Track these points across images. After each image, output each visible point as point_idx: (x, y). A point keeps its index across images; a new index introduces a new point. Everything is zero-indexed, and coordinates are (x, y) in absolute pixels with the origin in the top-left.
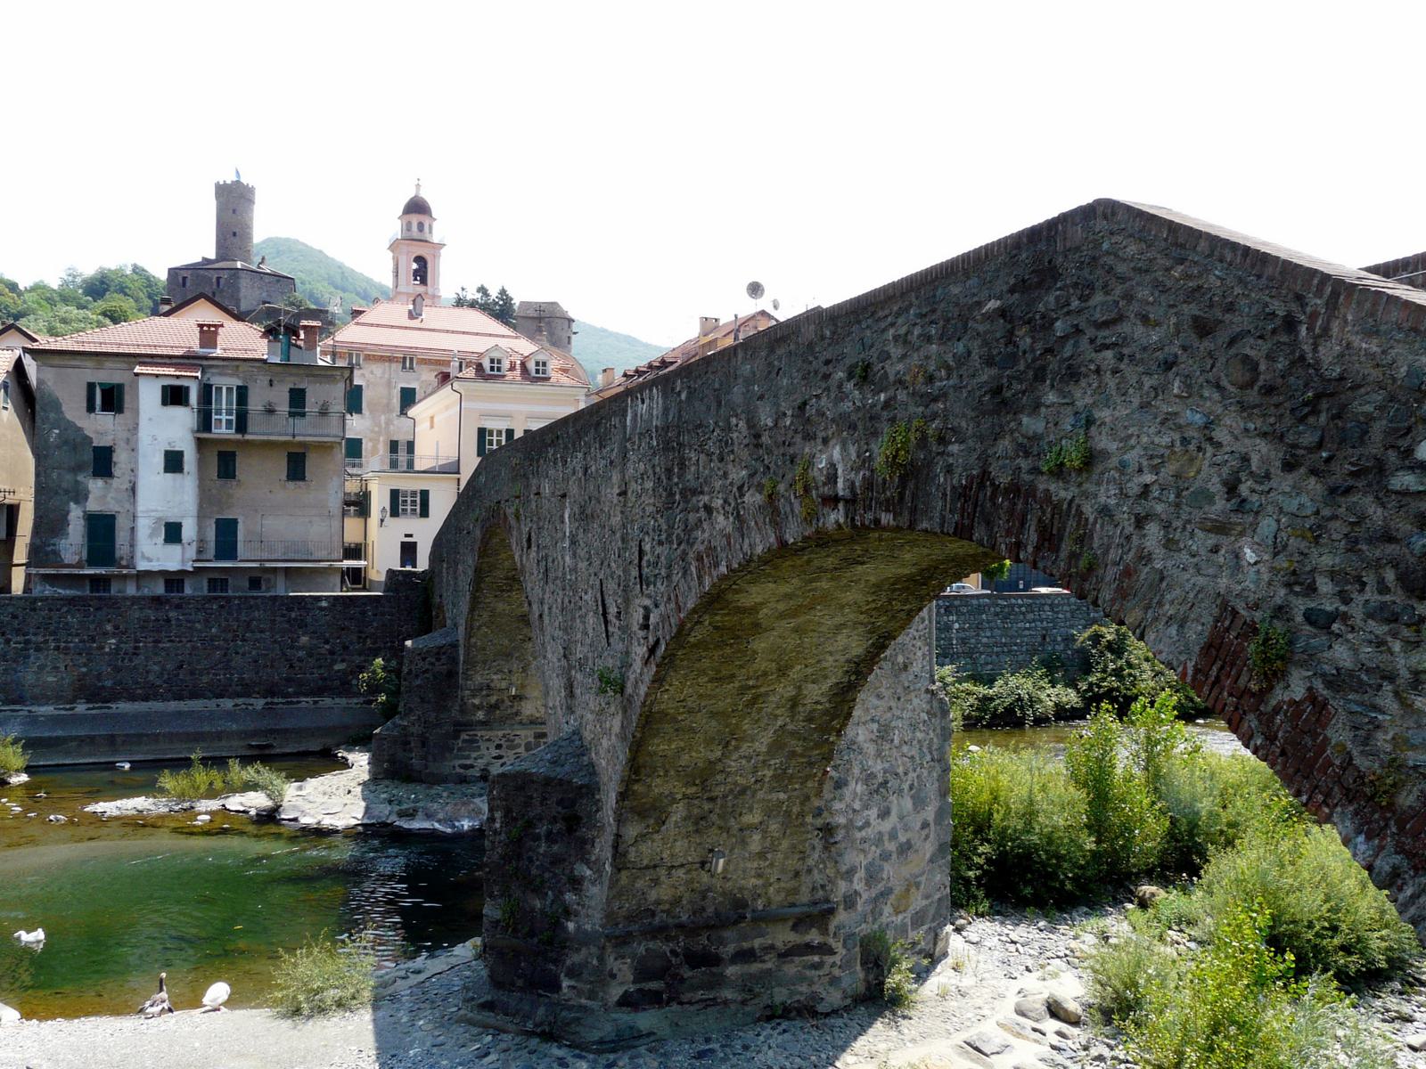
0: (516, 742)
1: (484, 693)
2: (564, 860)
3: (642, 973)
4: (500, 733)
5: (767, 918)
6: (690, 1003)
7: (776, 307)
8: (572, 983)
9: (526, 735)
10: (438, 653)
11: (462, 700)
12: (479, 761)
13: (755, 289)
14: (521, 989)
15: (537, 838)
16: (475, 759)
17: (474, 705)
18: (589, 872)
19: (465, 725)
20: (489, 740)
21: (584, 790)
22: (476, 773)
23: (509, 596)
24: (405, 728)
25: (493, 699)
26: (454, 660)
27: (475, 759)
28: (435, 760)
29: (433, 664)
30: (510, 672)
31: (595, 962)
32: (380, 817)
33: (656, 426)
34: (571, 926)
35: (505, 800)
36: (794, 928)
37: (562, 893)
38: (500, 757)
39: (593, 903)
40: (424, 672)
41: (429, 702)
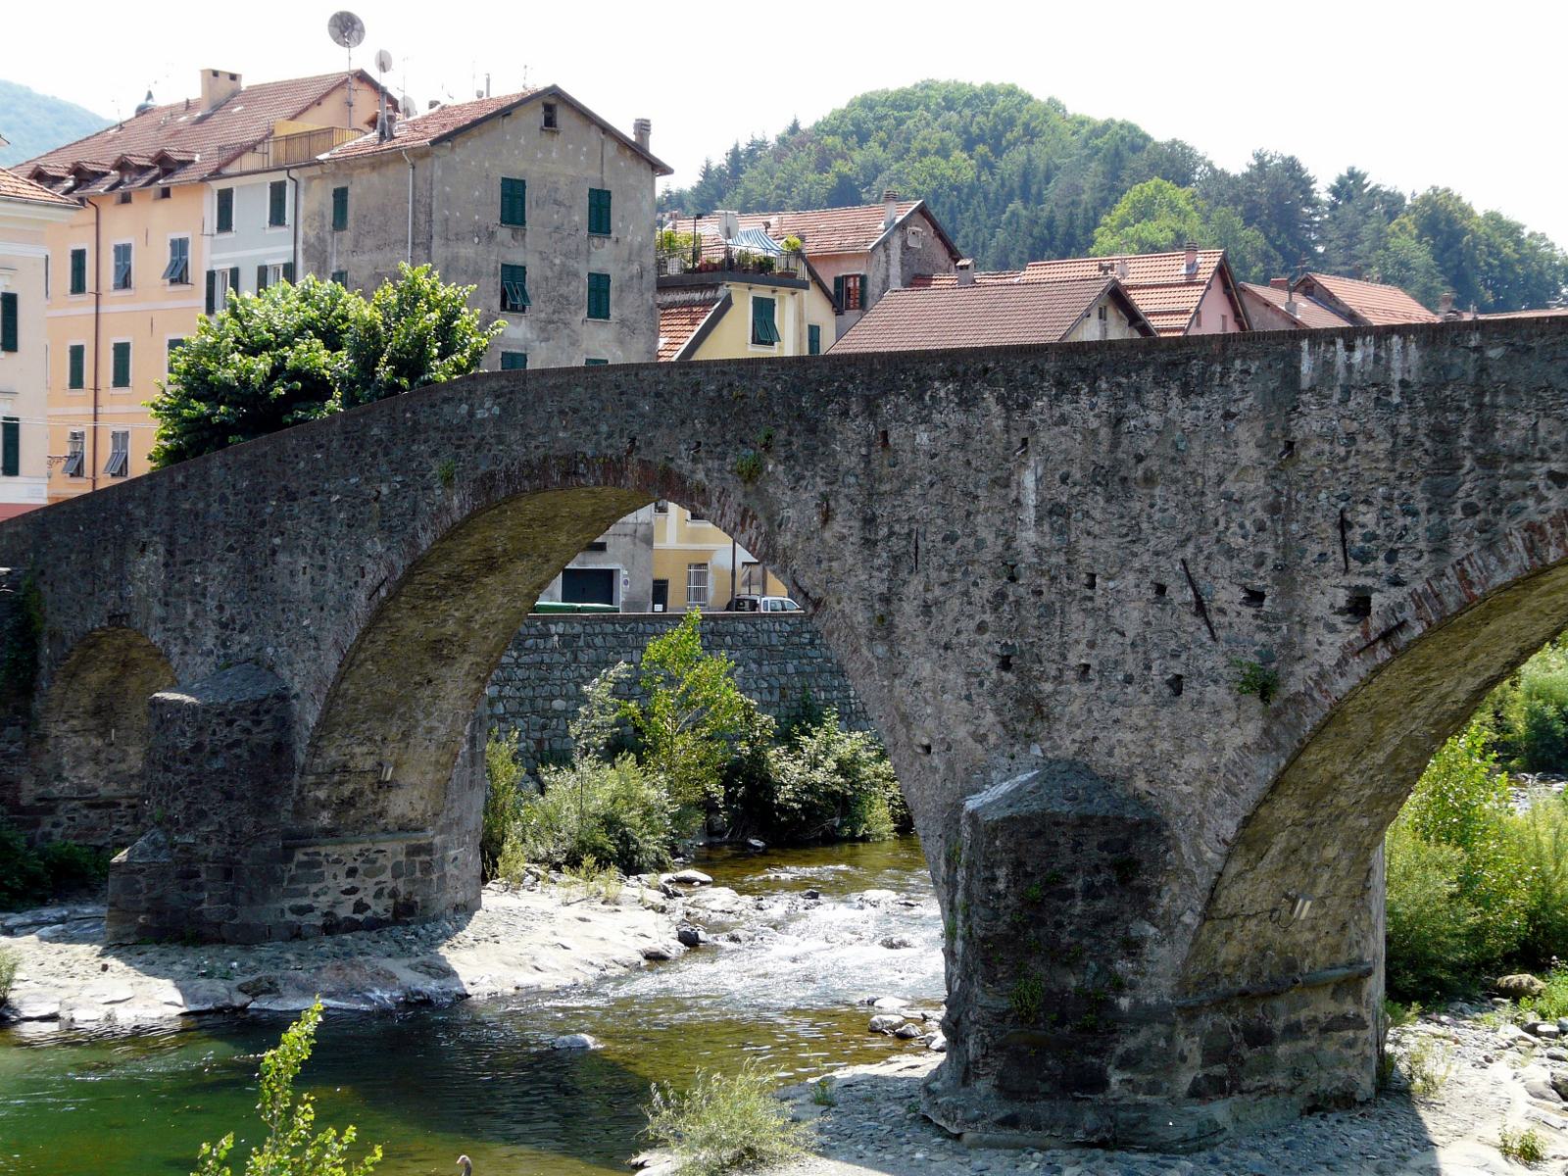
0: (378, 865)
1: (336, 778)
2: (1115, 919)
3: (1211, 1056)
4: (355, 849)
5: (1313, 984)
6: (1249, 1092)
7: (383, 66)
8: (1127, 1075)
9: (395, 849)
10: (256, 712)
11: (300, 792)
12: (322, 898)
13: (346, 27)
14: (1047, 1096)
15: (1070, 894)
16: (316, 895)
17: (317, 801)
18: (1152, 931)
19: (301, 837)
20: (337, 861)
21: (1143, 828)
22: (316, 920)
23: (433, 608)
24: (187, 848)
25: (347, 790)
26: (284, 724)
27: (316, 895)
28: (251, 900)
29: (248, 731)
30: (384, 739)
31: (1162, 1043)
32: (217, 999)
33: (1404, 383)
34: (1124, 1003)
35: (1015, 851)
36: (1334, 995)
37: (1110, 961)
38: (353, 891)
39: (1159, 968)
40: (229, 747)
41: (242, 798)
